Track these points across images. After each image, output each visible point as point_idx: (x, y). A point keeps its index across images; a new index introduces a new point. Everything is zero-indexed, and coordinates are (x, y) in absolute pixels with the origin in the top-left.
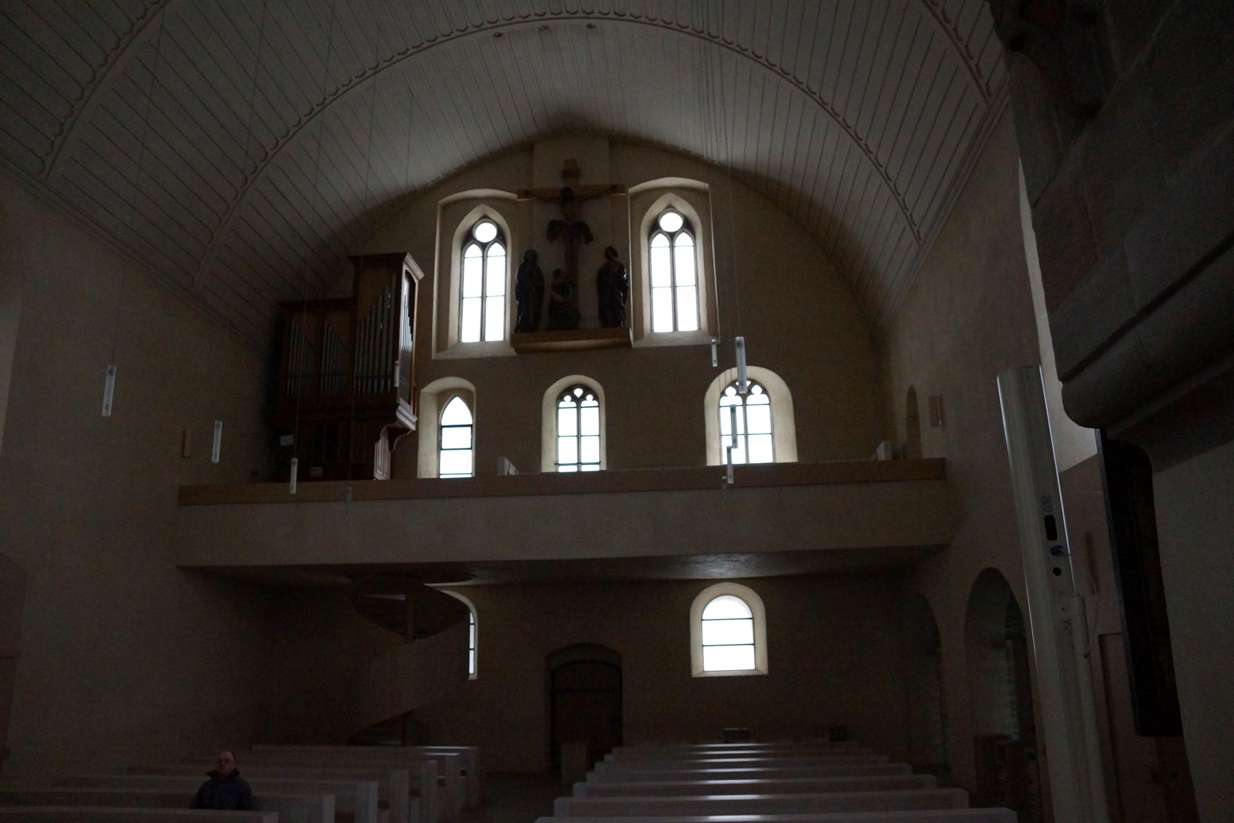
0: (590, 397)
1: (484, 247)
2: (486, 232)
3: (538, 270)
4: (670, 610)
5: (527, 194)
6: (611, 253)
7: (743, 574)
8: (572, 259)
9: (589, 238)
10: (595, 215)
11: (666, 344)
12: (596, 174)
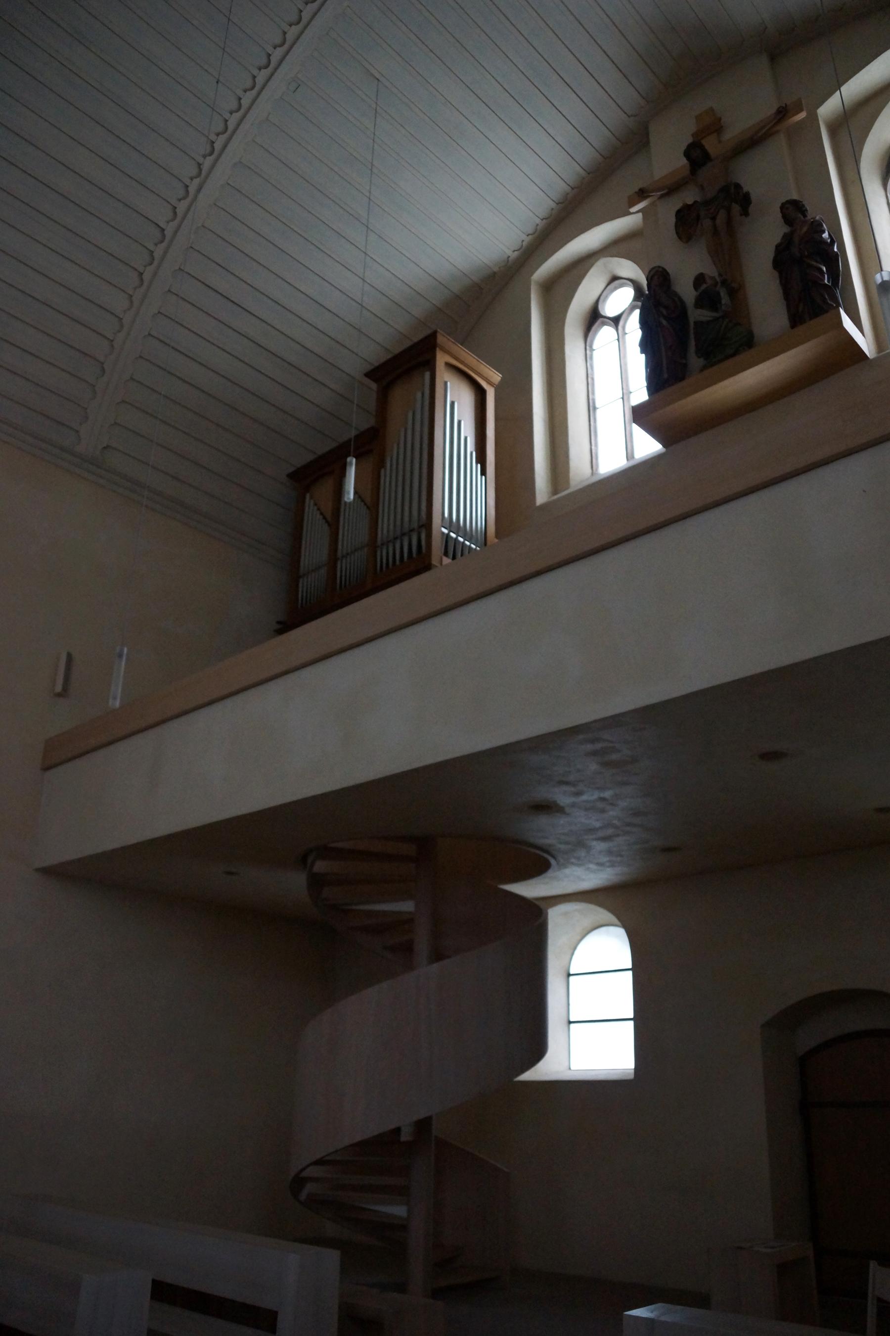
6: (793, 211)
10: (765, 178)
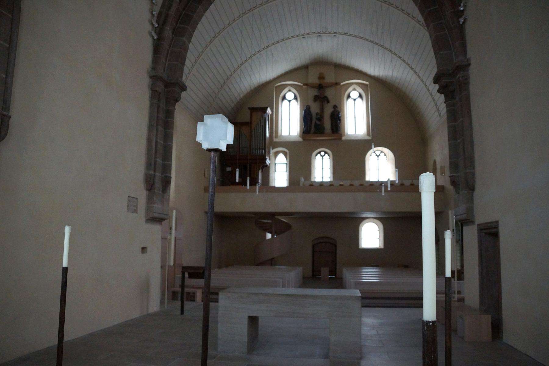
0: (326, 155)
1: (289, 101)
2: (290, 96)
3: (310, 112)
4: (353, 223)
5: (306, 85)
6: (335, 107)
7: (378, 216)
8: (322, 109)
9: (328, 102)
10: (329, 93)
11: (353, 139)
12: (330, 78)
